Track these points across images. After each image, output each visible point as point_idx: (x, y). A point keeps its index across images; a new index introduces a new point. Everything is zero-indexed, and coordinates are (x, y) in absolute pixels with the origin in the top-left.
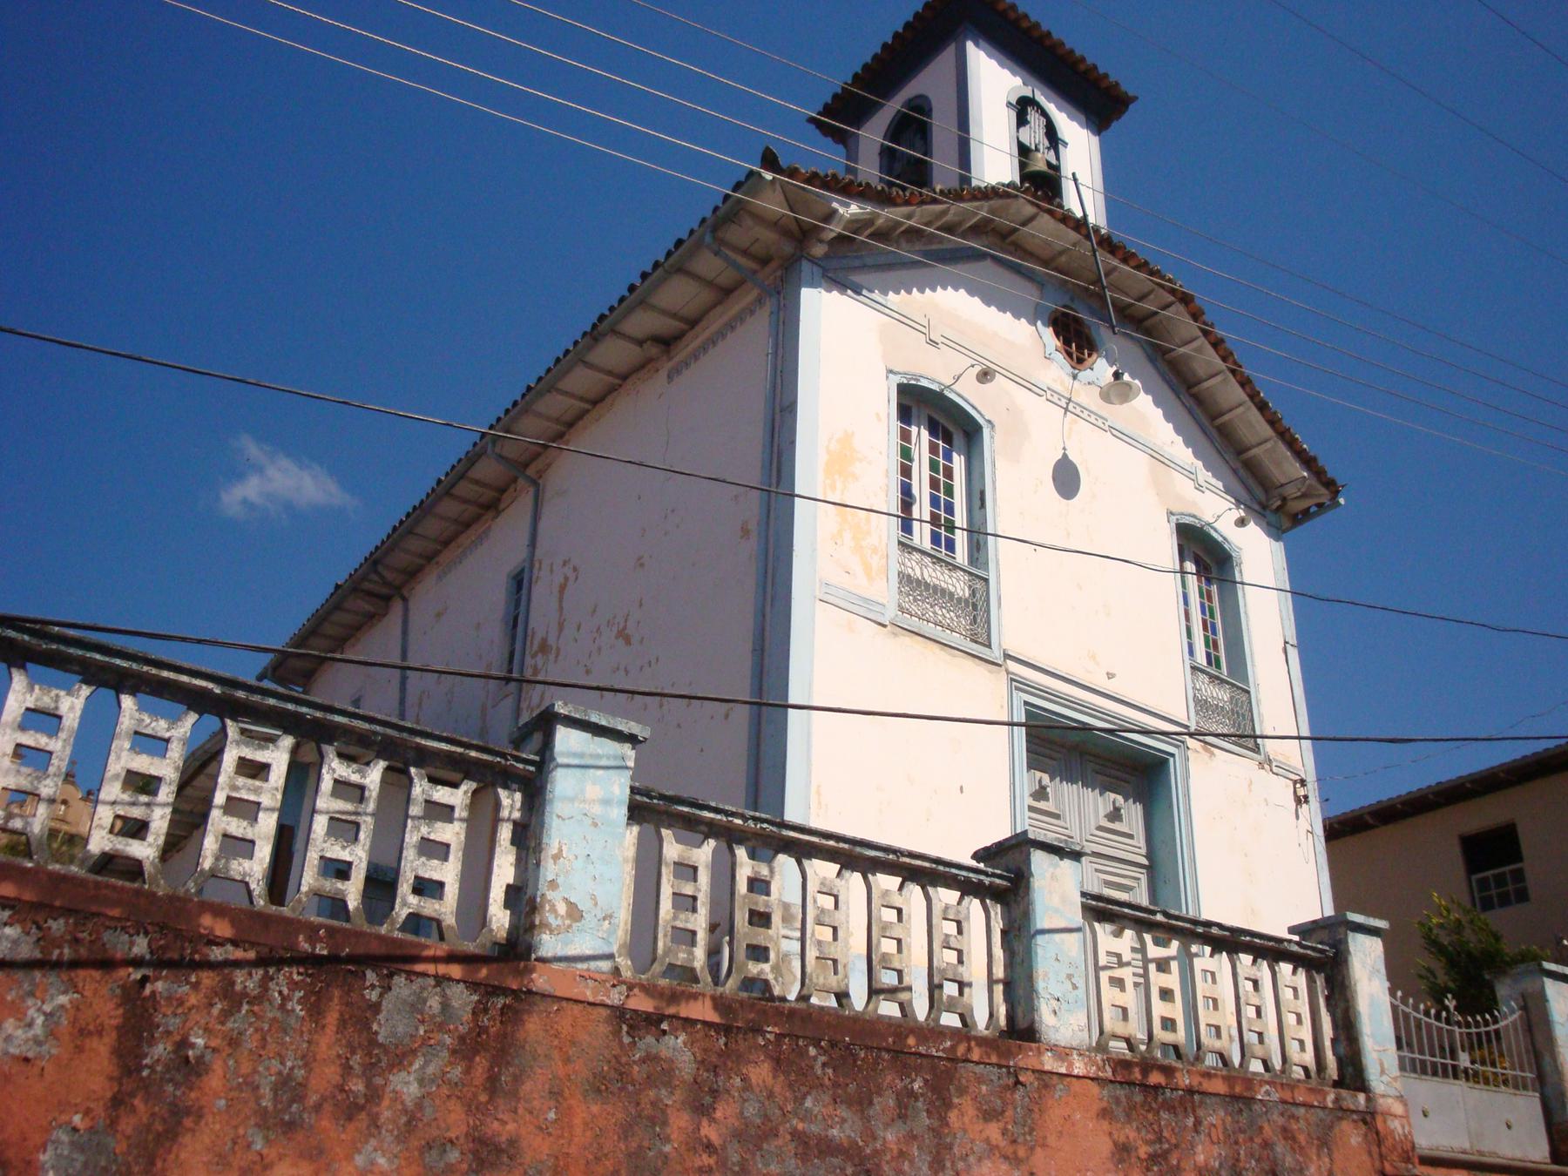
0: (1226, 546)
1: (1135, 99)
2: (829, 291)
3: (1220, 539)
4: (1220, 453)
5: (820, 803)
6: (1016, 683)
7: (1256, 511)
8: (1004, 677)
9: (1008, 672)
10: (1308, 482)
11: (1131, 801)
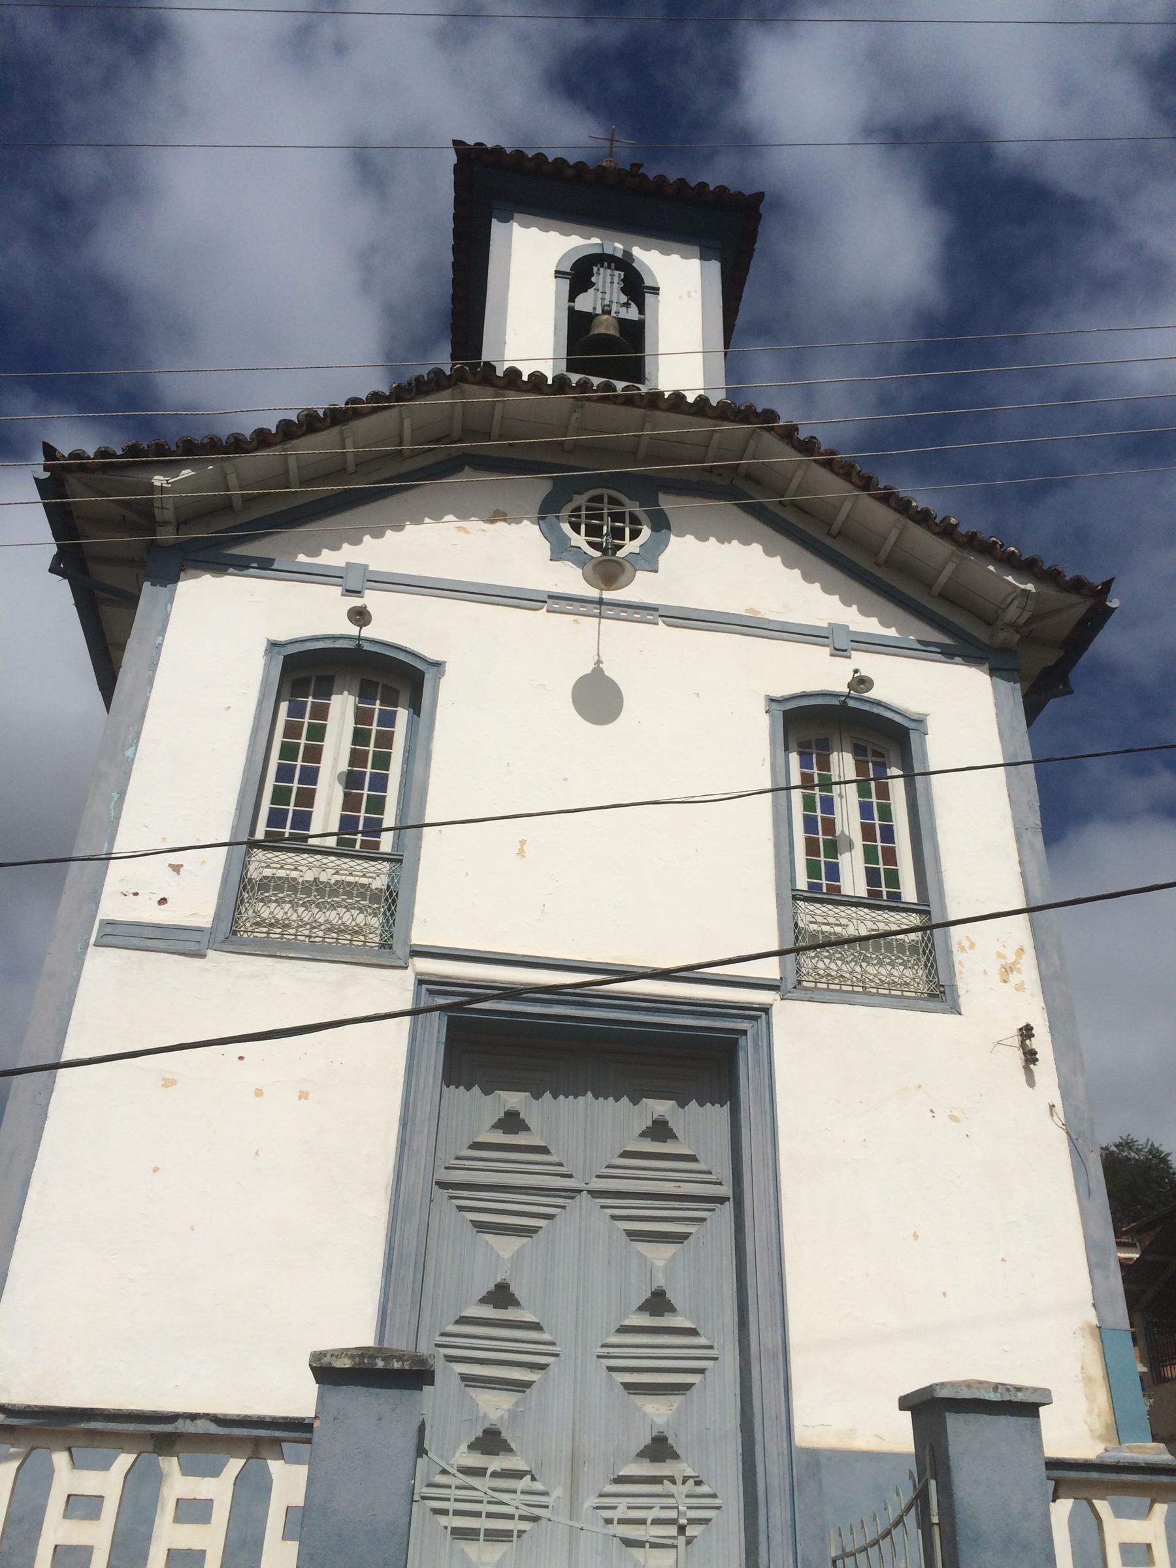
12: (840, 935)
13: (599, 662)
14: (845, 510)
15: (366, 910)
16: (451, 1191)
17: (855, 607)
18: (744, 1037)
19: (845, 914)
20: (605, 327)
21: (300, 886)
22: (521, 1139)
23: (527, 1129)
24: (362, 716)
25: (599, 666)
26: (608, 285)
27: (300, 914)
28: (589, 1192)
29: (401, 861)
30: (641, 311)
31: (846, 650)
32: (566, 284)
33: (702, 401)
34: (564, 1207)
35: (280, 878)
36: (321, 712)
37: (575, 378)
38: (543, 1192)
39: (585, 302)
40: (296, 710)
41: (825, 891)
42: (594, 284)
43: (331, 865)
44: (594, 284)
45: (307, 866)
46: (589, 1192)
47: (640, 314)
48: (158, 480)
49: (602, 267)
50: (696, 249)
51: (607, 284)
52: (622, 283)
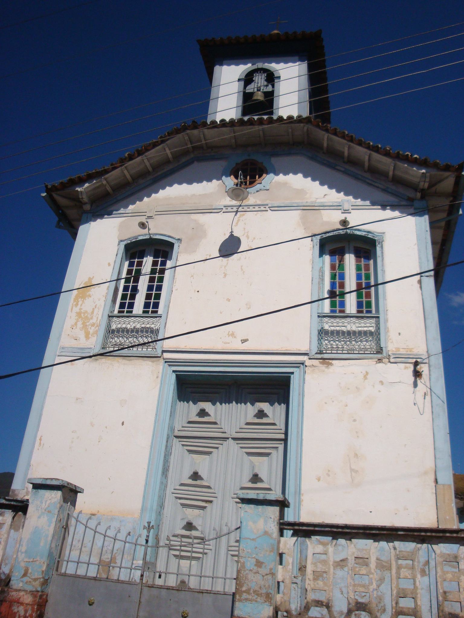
0: (370, 236)
1: (199, 41)
2: (95, 221)
3: (363, 234)
4: (371, 185)
5: (40, 444)
6: (170, 363)
7: (406, 206)
8: (162, 361)
9: (164, 359)
10: (428, 174)
11: (218, 404)
12: (327, 330)
13: (232, 232)
14: (148, 164)
15: (133, 336)
16: (180, 439)
17: (342, 193)
18: (293, 375)
19: (331, 321)
20: (259, 96)
21: (140, 330)
22: (264, 420)
23: (209, 415)
24: (155, 263)
25: (232, 233)
26: (260, 80)
27: (120, 340)
28: (232, 438)
29: (319, 316)
30: (273, 86)
31: (348, 210)
32: (242, 83)
33: (299, 116)
34: (222, 444)
35: (147, 328)
36: (140, 264)
37: (246, 118)
38: (221, 439)
39: (250, 88)
40: (131, 264)
41: (374, 313)
42: (254, 81)
43: (132, 321)
44: (254, 81)
45: (342, 323)
46: (232, 438)
47: (272, 88)
48: (79, 189)
49: (257, 73)
50: (297, 58)
51: (260, 80)
52: (265, 78)
